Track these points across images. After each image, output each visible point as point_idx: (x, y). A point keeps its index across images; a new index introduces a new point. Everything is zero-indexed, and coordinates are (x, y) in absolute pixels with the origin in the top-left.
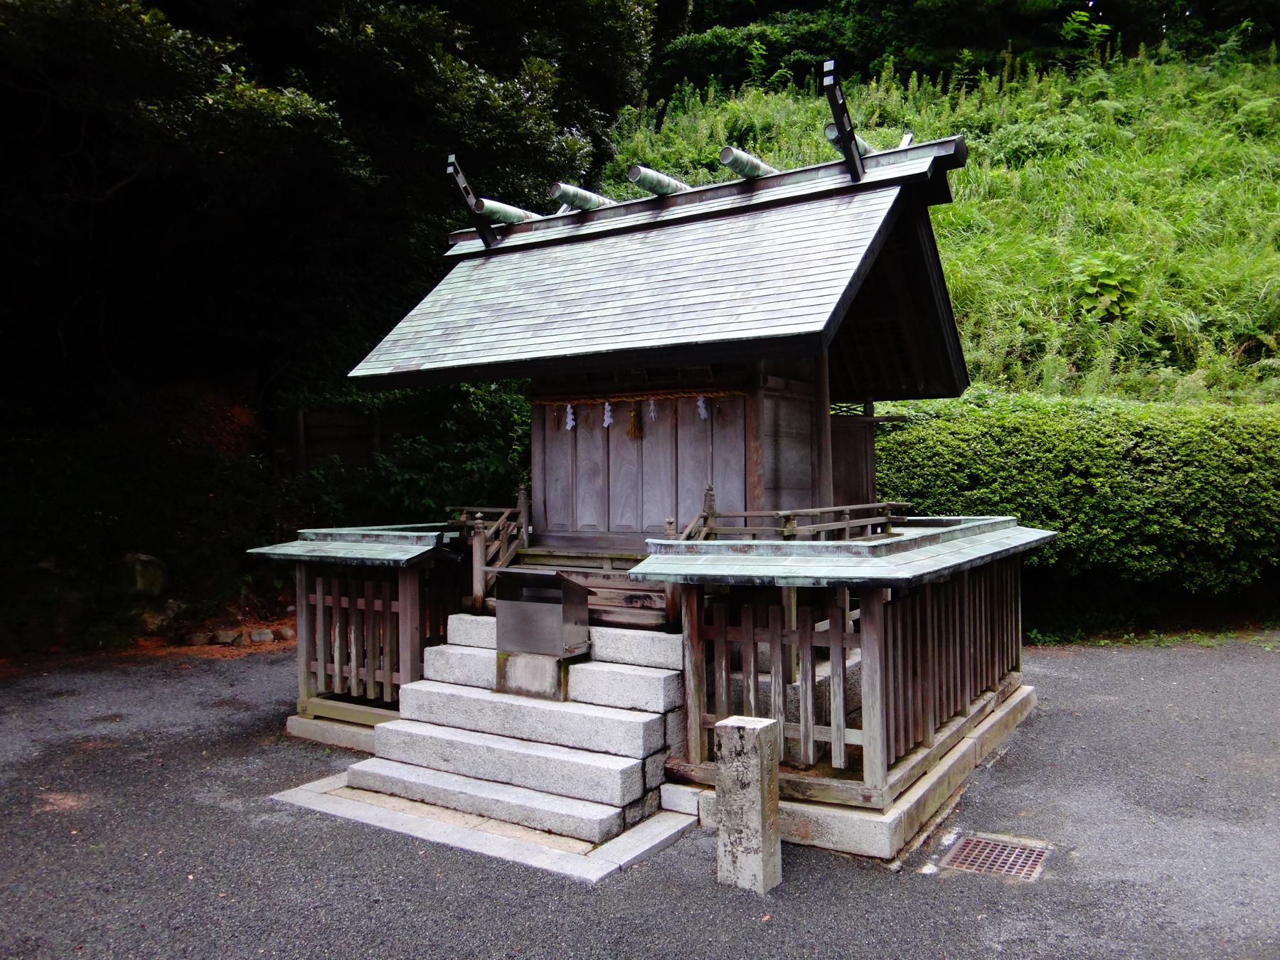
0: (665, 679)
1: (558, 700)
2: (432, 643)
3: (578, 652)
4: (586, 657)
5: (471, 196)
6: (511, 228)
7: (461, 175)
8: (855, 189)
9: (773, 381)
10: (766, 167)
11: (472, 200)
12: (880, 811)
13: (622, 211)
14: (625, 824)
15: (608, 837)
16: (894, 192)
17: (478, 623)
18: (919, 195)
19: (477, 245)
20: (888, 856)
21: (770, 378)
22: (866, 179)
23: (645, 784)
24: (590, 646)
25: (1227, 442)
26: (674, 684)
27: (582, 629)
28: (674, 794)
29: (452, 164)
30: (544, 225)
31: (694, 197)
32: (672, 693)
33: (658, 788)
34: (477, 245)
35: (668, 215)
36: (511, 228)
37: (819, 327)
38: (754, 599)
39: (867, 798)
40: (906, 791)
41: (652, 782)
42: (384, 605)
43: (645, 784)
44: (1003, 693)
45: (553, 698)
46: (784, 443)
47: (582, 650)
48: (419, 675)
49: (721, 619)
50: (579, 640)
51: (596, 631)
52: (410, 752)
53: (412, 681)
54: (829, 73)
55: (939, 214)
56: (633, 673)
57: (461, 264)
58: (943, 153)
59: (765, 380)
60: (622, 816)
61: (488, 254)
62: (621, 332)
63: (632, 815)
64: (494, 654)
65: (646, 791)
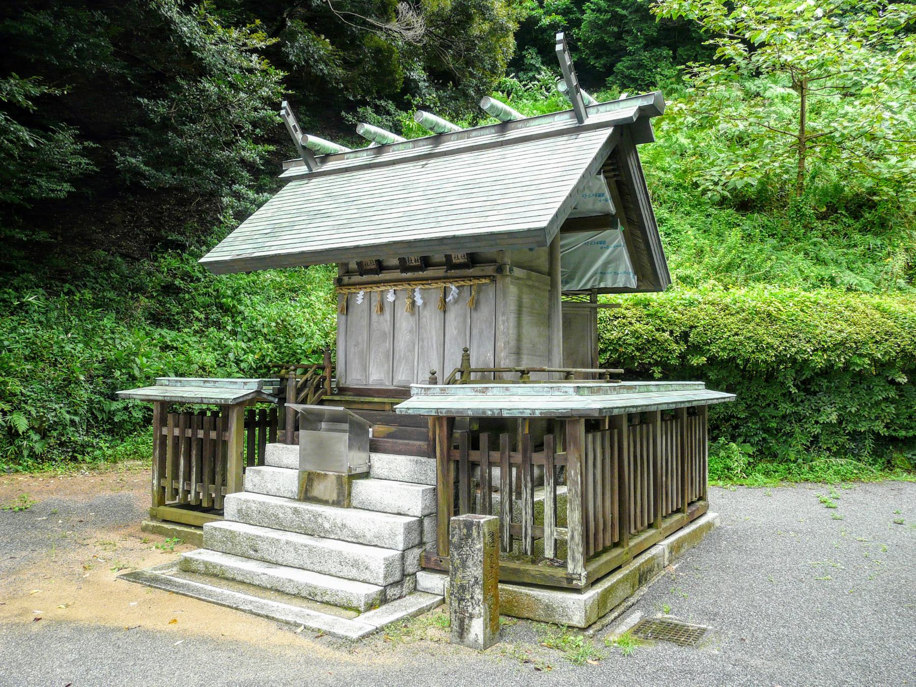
0: (423, 491)
1: (342, 507)
2: (251, 463)
3: (359, 471)
4: (366, 475)
5: (299, 132)
6: (327, 157)
7: (291, 116)
8: (580, 129)
9: (518, 272)
10: (516, 114)
11: (299, 136)
12: (577, 590)
13: (411, 145)
14: (383, 599)
15: (370, 606)
16: (609, 131)
17: (288, 449)
18: (629, 135)
19: (303, 169)
20: (582, 625)
21: (515, 269)
22: (587, 122)
23: (403, 570)
24: (370, 467)
25: (693, 89)
26: (430, 496)
27: (363, 455)
28: (427, 580)
29: (285, 108)
30: (352, 155)
31: (463, 135)
32: (428, 502)
33: (414, 574)
34: (303, 169)
35: (443, 148)
36: (327, 157)
37: (544, 224)
38: (493, 429)
39: (570, 580)
40: (555, 504)
41: (410, 570)
42: (218, 435)
43: (403, 570)
44: (692, 514)
45: (337, 504)
46: (526, 319)
47: (364, 469)
48: (240, 487)
49: (470, 448)
50: (361, 462)
51: (375, 457)
52: (229, 544)
53: (236, 492)
54: (560, 42)
55: (644, 152)
56: (399, 487)
57: (290, 184)
58: (645, 103)
59: (511, 270)
60: (383, 593)
61: (310, 176)
62: (401, 229)
63: (390, 592)
64: (295, 473)
65: (404, 575)
